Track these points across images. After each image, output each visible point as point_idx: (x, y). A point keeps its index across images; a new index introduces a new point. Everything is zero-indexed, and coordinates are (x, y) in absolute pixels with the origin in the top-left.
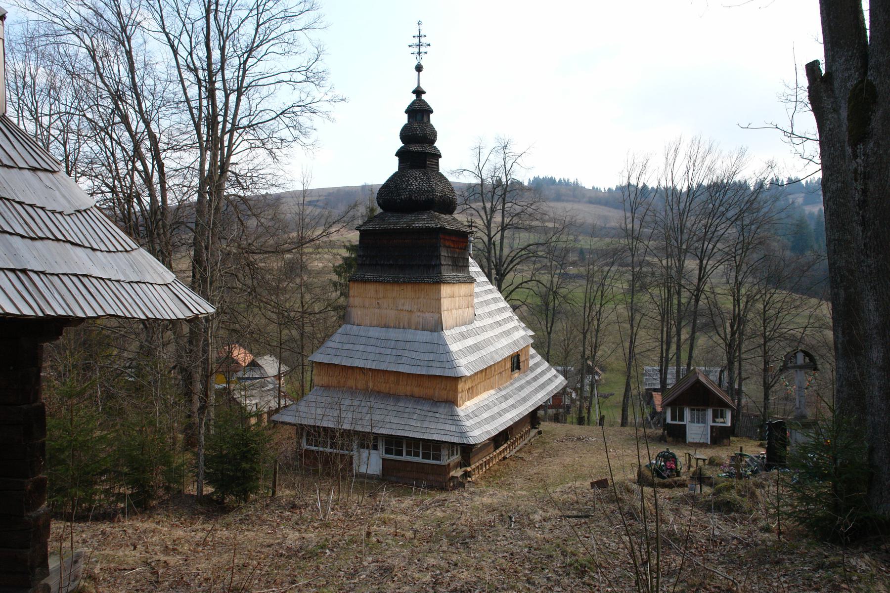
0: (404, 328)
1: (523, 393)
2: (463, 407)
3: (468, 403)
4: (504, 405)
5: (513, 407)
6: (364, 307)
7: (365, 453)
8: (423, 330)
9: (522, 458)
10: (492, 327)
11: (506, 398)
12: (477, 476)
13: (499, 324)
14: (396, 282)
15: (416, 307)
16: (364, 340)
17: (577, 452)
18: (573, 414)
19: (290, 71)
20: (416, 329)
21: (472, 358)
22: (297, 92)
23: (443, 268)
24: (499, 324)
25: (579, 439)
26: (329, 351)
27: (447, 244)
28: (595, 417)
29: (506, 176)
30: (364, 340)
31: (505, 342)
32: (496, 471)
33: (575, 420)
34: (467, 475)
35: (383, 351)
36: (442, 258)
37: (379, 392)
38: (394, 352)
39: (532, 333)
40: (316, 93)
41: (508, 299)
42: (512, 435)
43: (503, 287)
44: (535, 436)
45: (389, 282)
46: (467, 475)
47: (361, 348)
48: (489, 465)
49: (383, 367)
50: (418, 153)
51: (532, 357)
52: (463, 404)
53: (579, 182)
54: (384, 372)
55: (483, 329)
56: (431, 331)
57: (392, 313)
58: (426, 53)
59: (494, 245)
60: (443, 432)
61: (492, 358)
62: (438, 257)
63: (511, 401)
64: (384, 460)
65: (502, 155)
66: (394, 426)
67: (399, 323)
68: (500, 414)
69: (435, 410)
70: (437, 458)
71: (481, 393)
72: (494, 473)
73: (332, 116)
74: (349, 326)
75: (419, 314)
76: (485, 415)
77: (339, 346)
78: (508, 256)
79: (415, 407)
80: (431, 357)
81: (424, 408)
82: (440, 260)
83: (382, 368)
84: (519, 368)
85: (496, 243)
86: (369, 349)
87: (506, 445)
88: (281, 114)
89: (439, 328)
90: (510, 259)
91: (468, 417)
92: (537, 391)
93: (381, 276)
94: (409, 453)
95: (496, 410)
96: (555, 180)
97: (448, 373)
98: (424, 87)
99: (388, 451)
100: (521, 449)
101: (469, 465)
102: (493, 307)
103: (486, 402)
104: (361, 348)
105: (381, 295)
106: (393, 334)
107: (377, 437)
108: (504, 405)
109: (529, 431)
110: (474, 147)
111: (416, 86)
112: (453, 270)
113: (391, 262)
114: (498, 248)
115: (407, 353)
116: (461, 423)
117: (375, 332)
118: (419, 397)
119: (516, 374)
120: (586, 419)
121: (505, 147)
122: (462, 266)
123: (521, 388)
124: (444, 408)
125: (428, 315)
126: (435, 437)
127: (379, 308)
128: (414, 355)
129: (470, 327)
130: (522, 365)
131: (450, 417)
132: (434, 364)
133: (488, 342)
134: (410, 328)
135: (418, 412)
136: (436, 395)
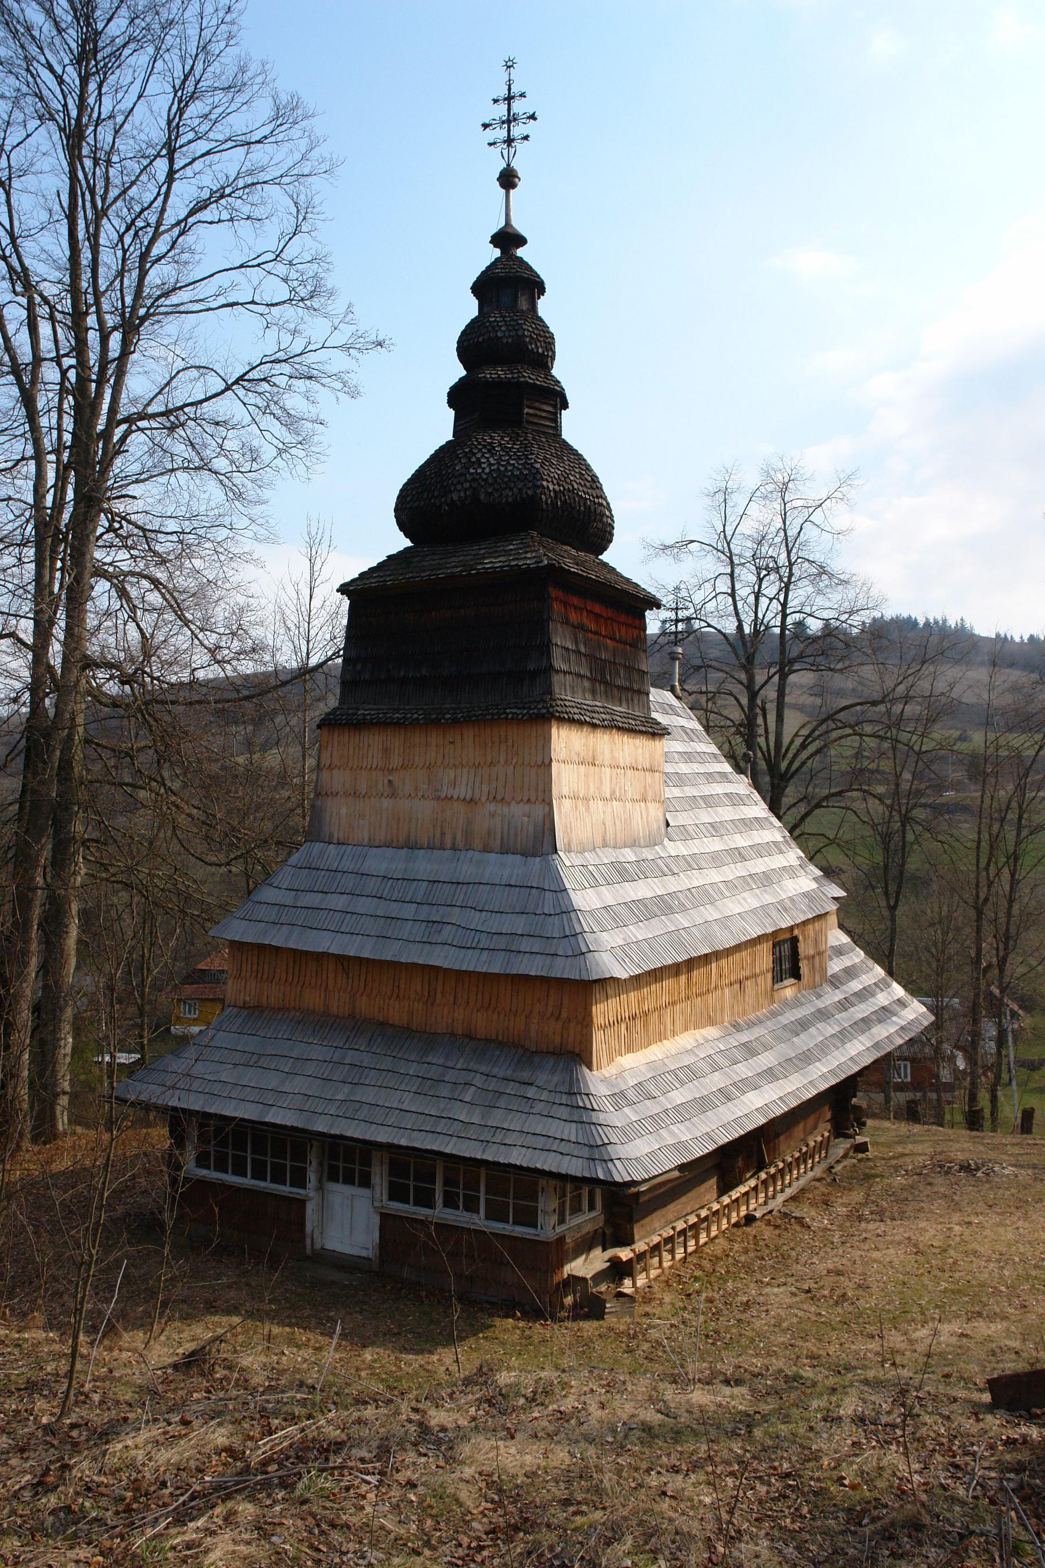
0: (454, 848)
1: (805, 1041)
2: (608, 1071)
3: (628, 1060)
4: (743, 1070)
5: (770, 1075)
6: (356, 794)
7: (340, 1193)
8: (505, 850)
9: (800, 1221)
10: (716, 859)
11: (750, 1050)
12: (653, 1273)
13: (739, 855)
14: (433, 722)
15: (485, 788)
16: (349, 882)
17: (957, 1207)
18: (956, 1110)
19: (241, 266)
20: (486, 849)
21: (638, 932)
22: (272, 333)
23: (557, 679)
24: (739, 855)
25: (965, 1168)
26: (262, 912)
27: (573, 617)
28: (1010, 1111)
29: (789, 553)
30: (349, 882)
31: (750, 901)
32: (715, 1259)
33: (959, 1117)
34: (618, 1270)
35: (394, 910)
36: (557, 654)
37: (383, 1024)
38: (424, 913)
39: (842, 893)
40: (317, 329)
41: (797, 832)
42: (774, 1152)
43: (786, 801)
44: (845, 1156)
45: (414, 724)
46: (618, 1270)
47: (339, 902)
48: (696, 1238)
49: (390, 952)
50: (498, 384)
51: (839, 951)
52: (611, 1060)
53: (967, 625)
54: (395, 966)
55: (691, 863)
56: (525, 854)
57: (425, 809)
58: (526, 138)
59: (764, 710)
60: (540, 1142)
61: (708, 937)
62: (545, 648)
63: (766, 1060)
64: (386, 1218)
65: (777, 506)
66: (409, 1122)
67: (443, 834)
68: (726, 1095)
69: (525, 1075)
70: (529, 1218)
71: (674, 1033)
72: (706, 1264)
73: (353, 379)
74: (318, 847)
75: (492, 807)
76: (679, 1096)
77: (289, 898)
78: (796, 735)
79: (472, 1065)
80: (520, 924)
81: (495, 1071)
82: (549, 657)
83: (388, 957)
84: (796, 974)
85: (768, 706)
86: (363, 905)
87: (752, 1183)
88: (236, 382)
89: (547, 847)
90: (798, 741)
91: (620, 1098)
92: (843, 1036)
93: (397, 710)
94: (450, 1202)
95: (716, 1081)
96: (915, 623)
97: (562, 969)
98: (520, 225)
99: (397, 1193)
100: (803, 1191)
101: (627, 1241)
102: (727, 813)
103: (687, 1060)
104: (339, 902)
105: (396, 761)
106: (424, 865)
107: (367, 1148)
108: (743, 1070)
109: (824, 1145)
110: (712, 490)
111: (502, 224)
112: (593, 692)
113: (424, 671)
114: (772, 718)
115: (455, 915)
116: (595, 1117)
117: (378, 862)
118: (488, 1040)
119: (789, 990)
120: (987, 1112)
121: (784, 488)
122: (620, 688)
123: (803, 1025)
124: (553, 1071)
125: (517, 810)
126: (517, 1157)
127: (393, 795)
128: (476, 920)
129: (647, 854)
130: (804, 967)
131: (564, 1099)
132: (525, 945)
133: (704, 896)
134: (469, 848)
135: (478, 1080)
136: (533, 1033)
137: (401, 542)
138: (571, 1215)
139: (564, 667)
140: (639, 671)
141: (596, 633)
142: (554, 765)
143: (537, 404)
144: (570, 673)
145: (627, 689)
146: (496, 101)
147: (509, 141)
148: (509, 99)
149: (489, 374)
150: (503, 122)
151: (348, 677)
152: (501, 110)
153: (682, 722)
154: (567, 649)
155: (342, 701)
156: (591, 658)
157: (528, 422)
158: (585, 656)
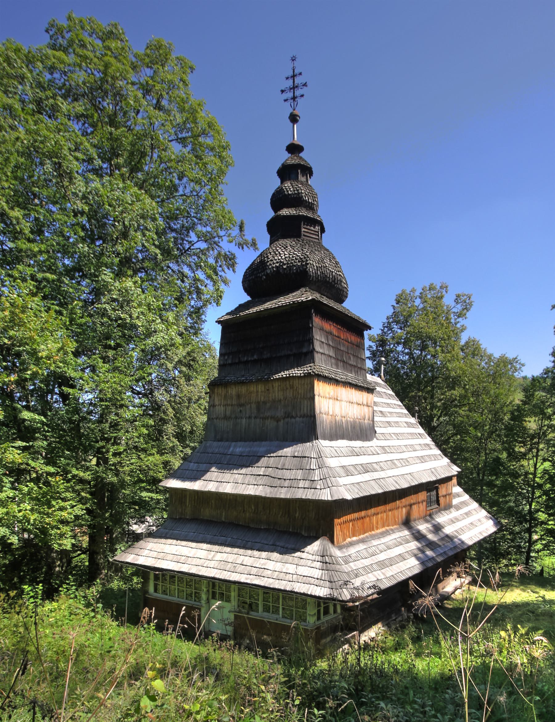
51: (458, 495)
58: (302, 96)
62: (311, 341)
93: (243, 376)
137: (246, 298)
138: (324, 615)
139: (321, 351)
140: (361, 358)
141: (338, 337)
142: (317, 398)
143: (308, 227)
144: (324, 354)
145: (355, 366)
146: (287, 78)
147: (294, 98)
148: (294, 76)
149: (285, 212)
150: (291, 89)
151: (222, 362)
152: (290, 83)
153: (384, 390)
154: (323, 342)
155: (219, 374)
156: (336, 349)
157: (304, 235)
158: (333, 347)
